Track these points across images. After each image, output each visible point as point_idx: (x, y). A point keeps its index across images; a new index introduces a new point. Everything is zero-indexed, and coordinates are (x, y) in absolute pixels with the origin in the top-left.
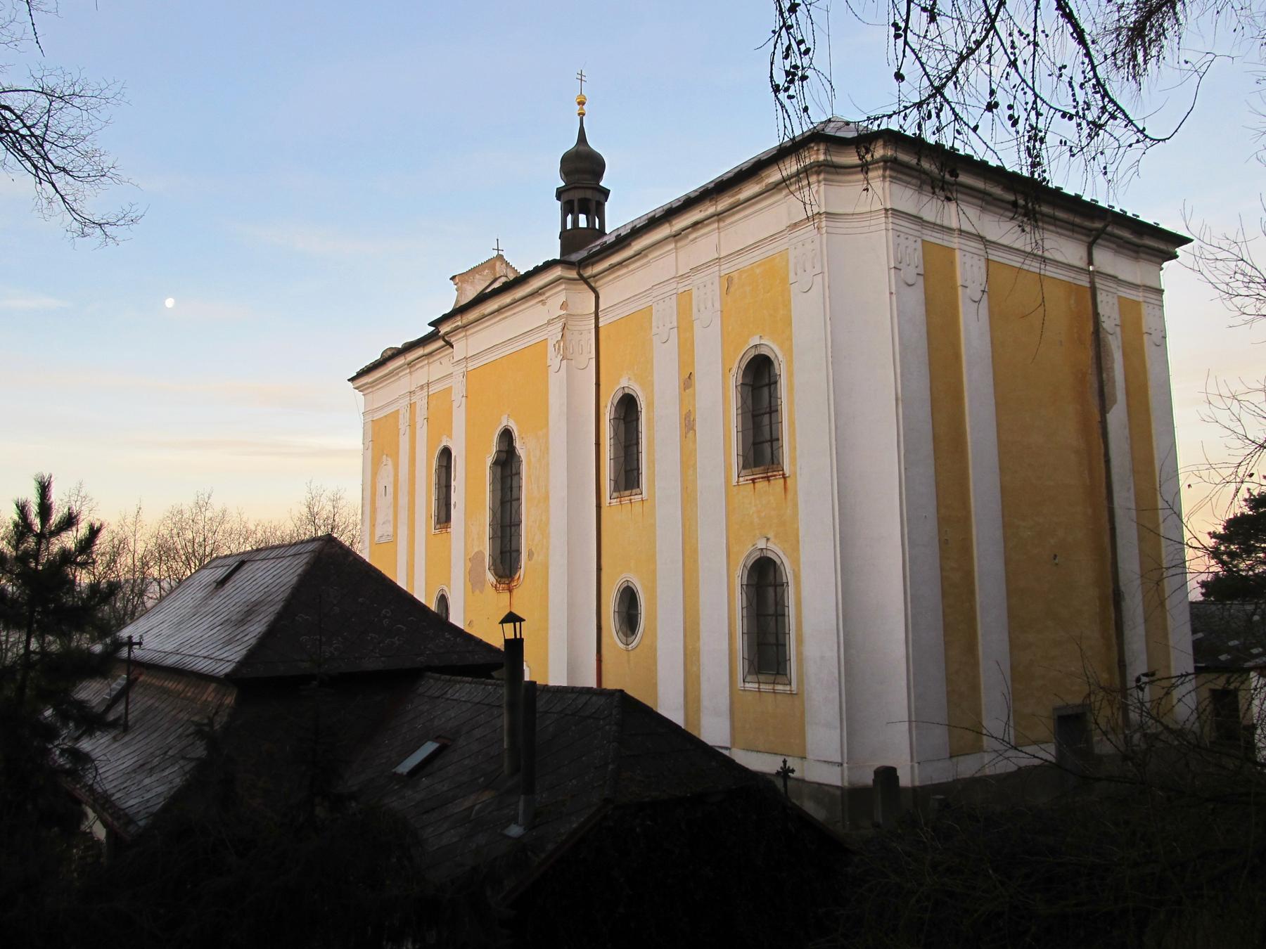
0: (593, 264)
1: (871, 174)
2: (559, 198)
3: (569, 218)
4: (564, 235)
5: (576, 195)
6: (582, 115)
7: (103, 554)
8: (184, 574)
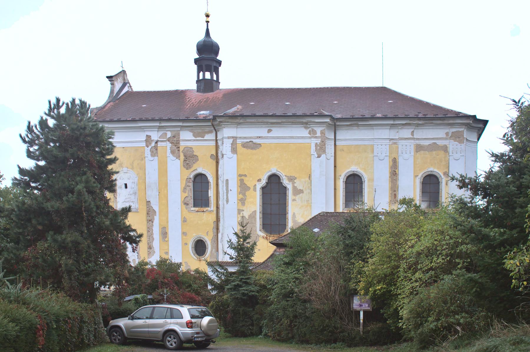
0: (340, 121)
1: (417, 153)
2: (196, 64)
3: (201, 73)
4: (198, 81)
5: (204, 63)
6: (208, 22)
7: (381, 234)
8: (410, 301)
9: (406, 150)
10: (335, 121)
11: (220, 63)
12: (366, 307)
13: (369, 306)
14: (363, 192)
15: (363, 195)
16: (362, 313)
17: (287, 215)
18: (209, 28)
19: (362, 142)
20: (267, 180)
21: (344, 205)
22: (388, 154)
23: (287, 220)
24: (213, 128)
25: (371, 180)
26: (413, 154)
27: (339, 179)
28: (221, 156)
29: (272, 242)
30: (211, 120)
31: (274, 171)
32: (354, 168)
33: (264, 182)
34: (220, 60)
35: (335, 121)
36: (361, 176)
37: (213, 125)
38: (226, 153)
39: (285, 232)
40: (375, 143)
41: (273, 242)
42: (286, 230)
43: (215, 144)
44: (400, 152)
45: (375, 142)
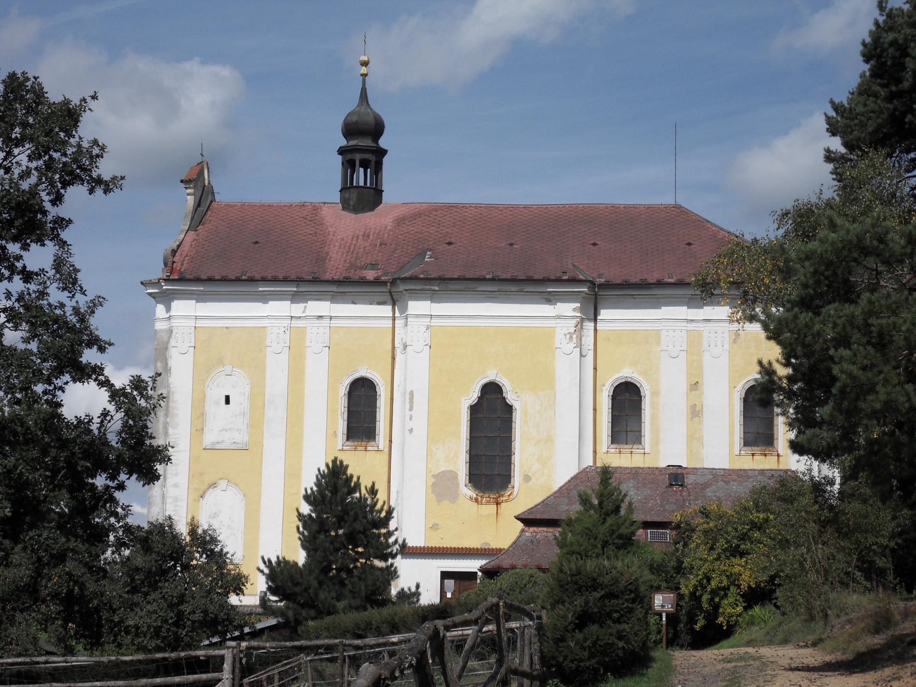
9: (716, 341)
10: (596, 290)
11: (383, 152)
12: (669, 608)
13: (672, 607)
14: (643, 416)
15: (643, 421)
16: (664, 615)
17: (512, 457)
18: (367, 86)
19: (643, 325)
20: (480, 393)
21: (610, 438)
22: (684, 348)
23: (512, 466)
24: (389, 297)
25: (655, 393)
26: (727, 347)
27: (602, 391)
28: (402, 347)
29: (518, 516)
30: (389, 284)
31: (490, 376)
32: (627, 373)
33: (474, 395)
34: (386, 149)
35: (596, 290)
36: (639, 385)
37: (390, 292)
38: (411, 344)
39: (508, 489)
40: (663, 328)
41: (520, 517)
42: (510, 486)
43: (391, 326)
44: (705, 344)
45: (662, 324)
